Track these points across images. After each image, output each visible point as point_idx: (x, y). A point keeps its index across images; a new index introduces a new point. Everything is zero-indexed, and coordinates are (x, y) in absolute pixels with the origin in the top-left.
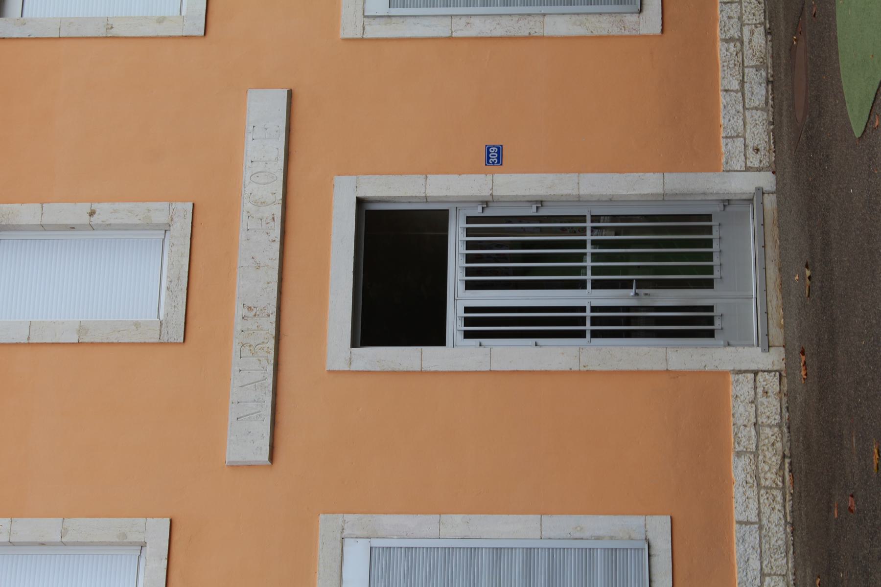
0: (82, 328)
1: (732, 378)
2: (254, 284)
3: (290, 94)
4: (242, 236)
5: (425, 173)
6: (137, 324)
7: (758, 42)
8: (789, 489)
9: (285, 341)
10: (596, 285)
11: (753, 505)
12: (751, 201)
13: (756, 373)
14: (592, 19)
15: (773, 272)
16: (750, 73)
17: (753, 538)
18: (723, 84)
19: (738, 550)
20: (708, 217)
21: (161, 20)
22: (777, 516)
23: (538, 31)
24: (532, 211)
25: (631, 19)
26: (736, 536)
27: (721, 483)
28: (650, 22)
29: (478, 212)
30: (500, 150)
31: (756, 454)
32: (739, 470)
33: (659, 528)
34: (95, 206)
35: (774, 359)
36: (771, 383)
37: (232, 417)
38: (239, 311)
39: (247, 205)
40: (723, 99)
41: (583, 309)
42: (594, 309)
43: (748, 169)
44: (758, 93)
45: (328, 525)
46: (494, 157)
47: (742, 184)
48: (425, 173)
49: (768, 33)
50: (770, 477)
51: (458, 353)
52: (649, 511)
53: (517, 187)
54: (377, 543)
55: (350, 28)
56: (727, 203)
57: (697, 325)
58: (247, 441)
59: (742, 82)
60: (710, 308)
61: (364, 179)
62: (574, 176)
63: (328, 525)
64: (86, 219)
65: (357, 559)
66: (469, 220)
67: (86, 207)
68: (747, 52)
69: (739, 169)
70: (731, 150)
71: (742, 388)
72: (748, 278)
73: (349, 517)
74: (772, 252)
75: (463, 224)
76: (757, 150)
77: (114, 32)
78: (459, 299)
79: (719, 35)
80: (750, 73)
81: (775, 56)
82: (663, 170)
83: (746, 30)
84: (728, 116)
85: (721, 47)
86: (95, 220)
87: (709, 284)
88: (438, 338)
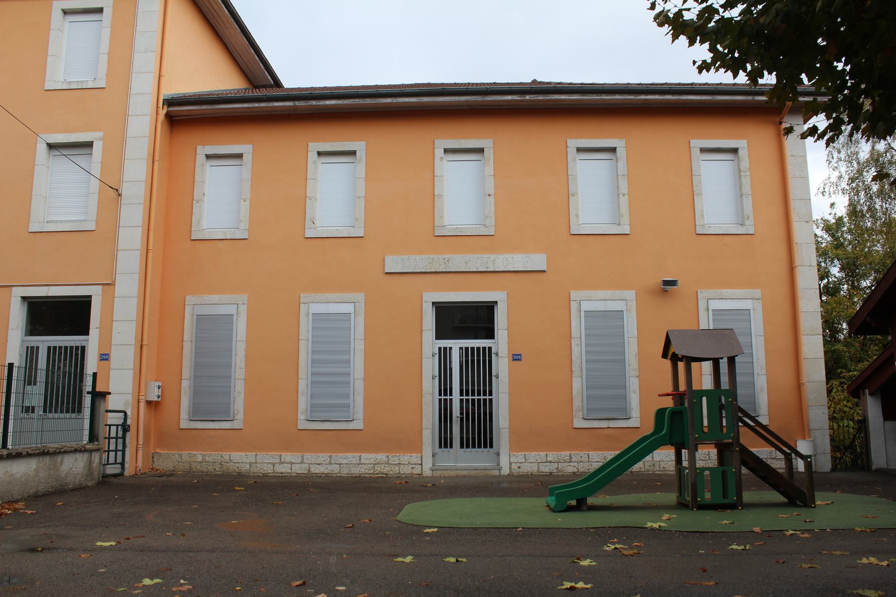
0: (440, 196)
1: (419, 455)
2: (458, 262)
3: (544, 271)
4: (479, 256)
5: (100, 328)
6: (442, 217)
7: (570, 469)
8: (374, 476)
9: (435, 276)
10: (461, 400)
11: (367, 462)
12: (499, 465)
13: (421, 464)
14: (580, 398)
15: (466, 473)
16: (556, 465)
17: (354, 461)
18: (550, 454)
19: (350, 455)
20: (491, 446)
21: (577, 216)
22: (363, 471)
23: (575, 375)
24: (494, 373)
25: (581, 415)
26: (542, 454)
27: (377, 449)
28: (579, 423)
29: (493, 351)
30: (520, 360)
31: (388, 463)
32: (381, 457)
33: (358, 425)
34: (493, 196)
35: (427, 472)
36: (417, 470)
37: (403, 257)
38: (447, 256)
39: (493, 257)
40: (543, 454)
41: (451, 395)
42: (451, 400)
43: (510, 464)
44: (545, 469)
45: (360, 297)
46: (516, 358)
47: (504, 461)
48: (508, 329)
49: (574, 473)
50: (378, 469)
51: (431, 344)
52: (365, 420)
53: (502, 366)
54: (235, 317)
55: (574, 295)
56: (498, 454)
57: (445, 442)
58: (393, 263)
59: (551, 462)
60: (451, 447)
61: (505, 304)
62: (507, 390)
63: (360, 297)
64: (621, 192)
65: (348, 308)
66: (490, 348)
67: (492, 192)
68: (565, 465)
69: (508, 459)
70: (519, 457)
71: (415, 458)
72: (465, 461)
73: (363, 304)
74: (473, 473)
75: (487, 346)
76: (519, 468)
77: (571, 198)
78: (456, 345)
79: (573, 453)
80: (556, 465)
81: (216, 475)
82: (510, 428)
83: (576, 464)
84: (533, 456)
85: (568, 453)
86: (621, 196)
87: (462, 446)
88: (439, 336)
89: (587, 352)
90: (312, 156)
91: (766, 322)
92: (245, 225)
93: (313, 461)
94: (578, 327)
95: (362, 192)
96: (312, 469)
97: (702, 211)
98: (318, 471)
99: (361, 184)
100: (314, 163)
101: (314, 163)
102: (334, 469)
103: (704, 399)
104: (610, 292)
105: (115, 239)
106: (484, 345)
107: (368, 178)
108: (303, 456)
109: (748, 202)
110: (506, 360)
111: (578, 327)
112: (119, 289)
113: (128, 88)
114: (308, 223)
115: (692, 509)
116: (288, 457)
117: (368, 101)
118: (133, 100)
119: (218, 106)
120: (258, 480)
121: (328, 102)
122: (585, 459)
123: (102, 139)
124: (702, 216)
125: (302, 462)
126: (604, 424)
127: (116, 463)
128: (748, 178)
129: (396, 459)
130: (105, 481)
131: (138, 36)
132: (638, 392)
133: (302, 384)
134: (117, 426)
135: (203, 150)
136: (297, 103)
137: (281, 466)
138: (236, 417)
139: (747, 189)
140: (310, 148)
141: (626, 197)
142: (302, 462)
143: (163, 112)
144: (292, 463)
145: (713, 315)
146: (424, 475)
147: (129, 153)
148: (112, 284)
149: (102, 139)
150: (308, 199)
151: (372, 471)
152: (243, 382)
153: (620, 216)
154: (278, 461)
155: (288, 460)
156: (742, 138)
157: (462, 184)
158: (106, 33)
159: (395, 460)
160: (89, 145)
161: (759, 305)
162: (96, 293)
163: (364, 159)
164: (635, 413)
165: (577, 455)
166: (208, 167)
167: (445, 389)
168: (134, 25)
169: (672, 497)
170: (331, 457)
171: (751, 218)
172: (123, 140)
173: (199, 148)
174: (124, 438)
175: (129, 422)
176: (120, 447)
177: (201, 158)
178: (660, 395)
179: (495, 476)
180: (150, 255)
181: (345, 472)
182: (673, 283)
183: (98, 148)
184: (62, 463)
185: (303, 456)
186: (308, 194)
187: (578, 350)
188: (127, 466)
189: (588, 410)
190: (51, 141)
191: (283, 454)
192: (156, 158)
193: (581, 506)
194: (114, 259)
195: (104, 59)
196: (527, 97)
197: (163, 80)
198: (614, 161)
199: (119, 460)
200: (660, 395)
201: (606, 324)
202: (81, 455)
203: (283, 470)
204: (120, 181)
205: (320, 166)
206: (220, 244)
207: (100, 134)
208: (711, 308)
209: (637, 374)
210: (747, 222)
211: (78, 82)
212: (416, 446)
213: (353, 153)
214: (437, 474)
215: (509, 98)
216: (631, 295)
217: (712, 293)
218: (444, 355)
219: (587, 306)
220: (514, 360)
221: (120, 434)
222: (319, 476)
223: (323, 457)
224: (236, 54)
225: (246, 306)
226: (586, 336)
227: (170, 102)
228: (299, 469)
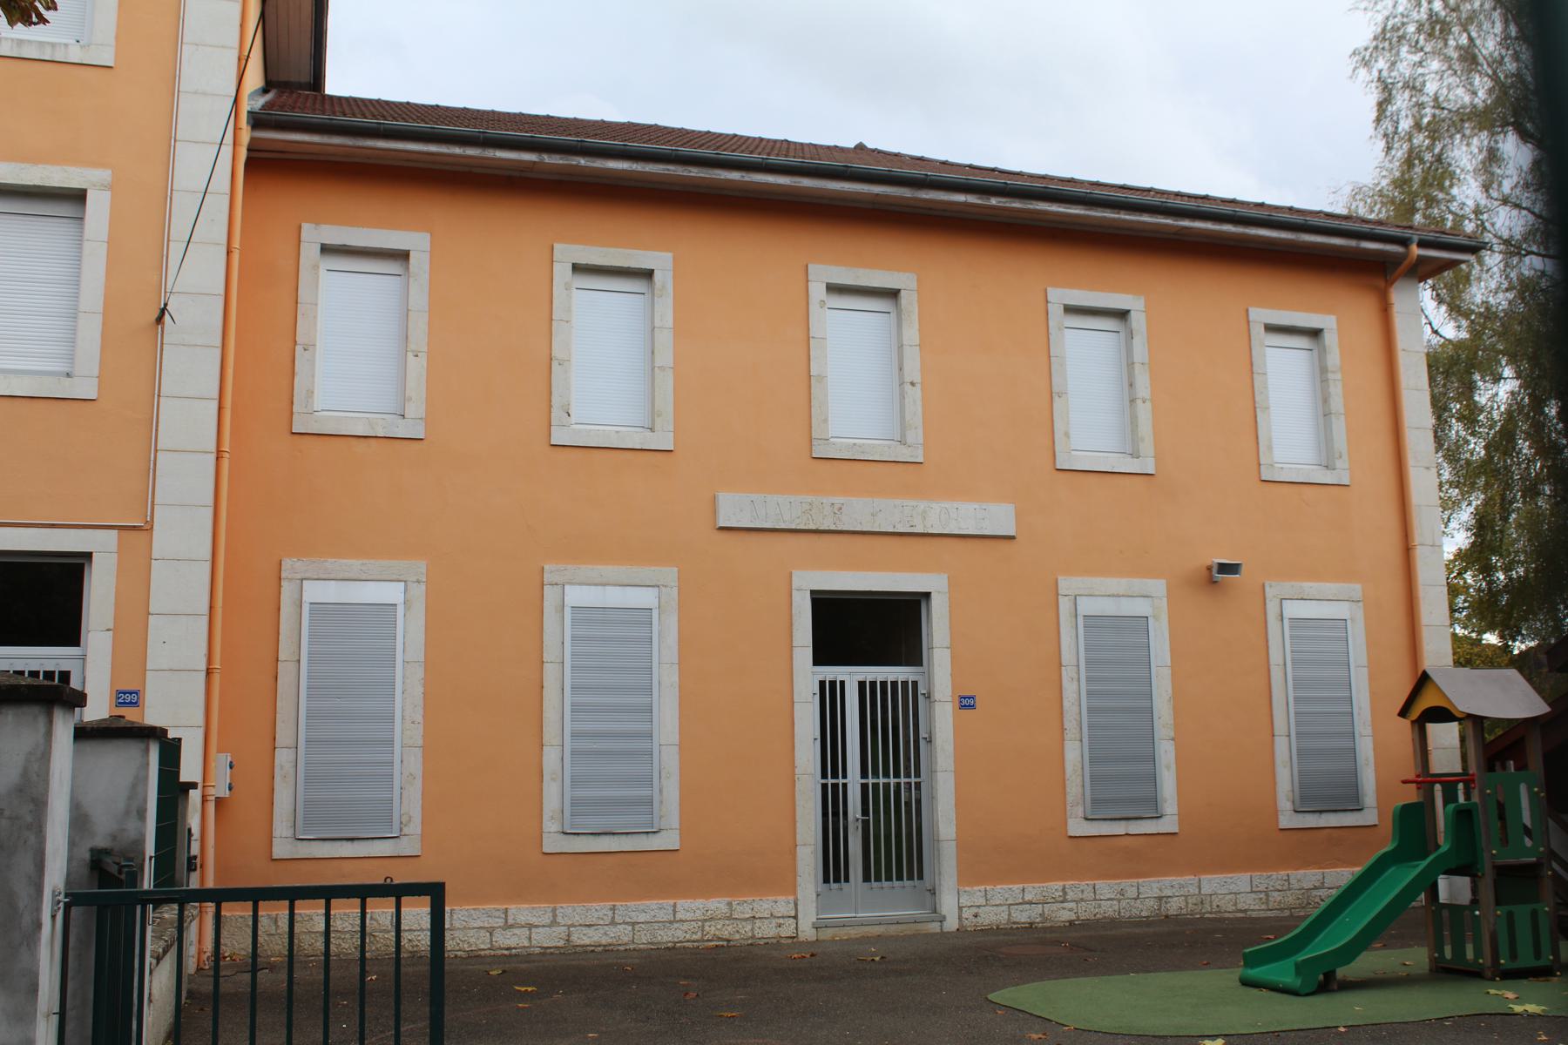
0: (822, 378)
1: (791, 898)
2: (861, 512)
3: (1012, 538)
4: (898, 502)
5: (115, 630)
6: (826, 421)
8: (702, 945)
10: (864, 787)
11: (689, 916)
13: (795, 917)
14: (1079, 780)
18: (1029, 887)
19: (653, 904)
20: (921, 877)
21: (1067, 435)
22: (680, 935)
23: (1069, 735)
24: (923, 734)
25: (1080, 811)
27: (706, 891)
28: (1078, 827)
29: (922, 690)
30: (972, 707)
31: (729, 918)
32: (717, 905)
33: (669, 840)
34: (918, 386)
35: (807, 932)
36: (788, 930)
37: (754, 496)
38: (838, 500)
39: (922, 505)
40: (1016, 887)
41: (845, 776)
42: (845, 785)
43: (960, 908)
44: (1022, 916)
45: (670, 574)
46: (966, 703)
47: (948, 904)
49: (1071, 922)
51: (807, 676)
52: (684, 832)
53: (942, 720)
54: (655, 614)
55: (1067, 584)
56: (933, 892)
57: (833, 869)
58: (735, 509)
59: (1031, 903)
60: (847, 880)
63: (670, 574)
64: (908, 379)
65: (390, 593)
66: (915, 684)
68: (1055, 907)
69: (961, 901)
70: (975, 895)
71: (783, 906)
72: (873, 911)
73: (675, 590)
76: (976, 916)
78: (851, 676)
83: (1072, 905)
85: (1058, 885)
86: (908, 387)
87: (866, 878)
88: (818, 660)
89: (1089, 693)
91: (1370, 644)
92: (416, 409)
93: (577, 919)
94: (1071, 647)
96: (574, 938)
97: (1270, 440)
98: (587, 942)
100: (568, 287)
101: (568, 287)
102: (620, 935)
103: (1438, 787)
104: (1124, 581)
105: (151, 423)
108: (554, 910)
109: (1339, 427)
110: (949, 708)
111: (1071, 647)
112: (162, 541)
114: (556, 414)
115: (1493, 979)
116: (521, 912)
117: (694, 172)
118: (186, 105)
121: (613, 164)
122: (1089, 895)
123: (111, 187)
124: (1270, 448)
125: (554, 923)
126: (1119, 828)
128: (1339, 385)
129: (747, 908)
132: (1174, 767)
133: (551, 758)
137: (509, 933)
138: (406, 831)
139: (1337, 403)
141: (1148, 404)
142: (554, 923)
144: (531, 926)
145: (1291, 628)
146: (802, 937)
148: (147, 529)
151: (697, 937)
152: (419, 752)
153: (405, 399)
154: (501, 922)
155: (522, 919)
156: (1329, 311)
157: (859, 351)
159: (743, 911)
161: (1360, 615)
162: (102, 547)
164: (1170, 806)
165: (1079, 888)
167: (831, 761)
169: (1417, 957)
170: (613, 909)
171: (1345, 456)
178: (1404, 782)
179: (933, 935)
180: (225, 464)
181: (643, 939)
182: (1226, 568)
183: (98, 206)
185: (554, 910)
187: (1073, 690)
189: (1094, 801)
191: (513, 908)
193: (1327, 983)
194: (149, 471)
196: (994, 201)
198: (893, 315)
200: (1404, 782)
201: (1117, 639)
203: (512, 942)
206: (360, 446)
207: (104, 175)
208: (1082, 610)
209: (1172, 734)
210: (1339, 464)
211: (41, 43)
212: (784, 882)
214: (827, 934)
215: (960, 198)
216: (1158, 587)
217: (1287, 587)
218: (830, 695)
219: (1088, 607)
220: (963, 707)
222: (587, 951)
223: (598, 910)
225: (423, 587)
226: (1088, 662)
228: (547, 938)
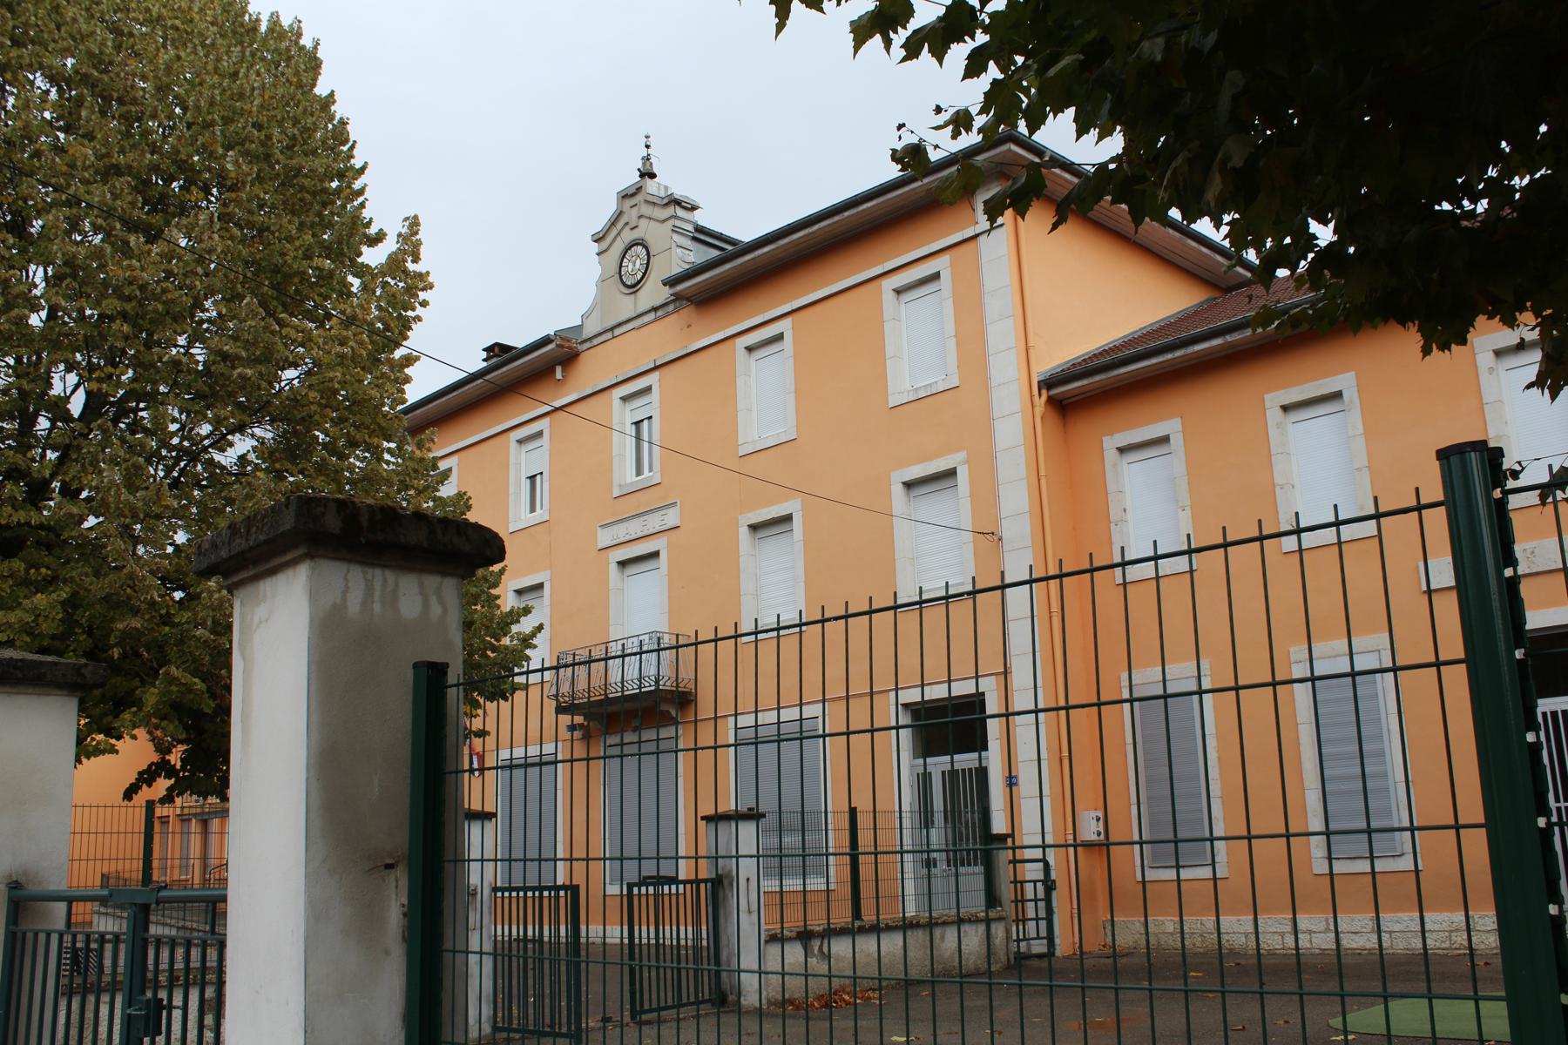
11: (1436, 927)
90: (1274, 415)
95: (1363, 460)
99: (1360, 444)
101: (1279, 426)
106: (1553, 708)
107: (1369, 432)
113: (986, 379)
119: (1116, 372)
120: (1243, 962)
123: (967, 461)
127: (1038, 938)
130: (1020, 962)
131: (987, 298)
134: (1035, 882)
135: (1111, 443)
136: (1229, 338)
140: (1268, 404)
143: (1041, 402)
147: (1003, 475)
149: (967, 461)
150: (1278, 490)
151: (1447, 945)
158: (948, 305)
160: (951, 473)
163: (1357, 401)
166: (1125, 466)
168: (979, 285)
172: (991, 457)
173: (1106, 439)
174: (1048, 900)
175: (1053, 876)
176: (1042, 914)
177: (1111, 455)
183: (963, 474)
184: (943, 938)
186: (1278, 480)
188: (1057, 941)
190: (907, 479)
192: (1042, 473)
195: (952, 344)
197: (1031, 352)
199: (1043, 933)
202: (974, 927)
204: (997, 520)
205: (1291, 428)
207: (962, 455)
213: (1337, 396)
221: (1041, 894)
224: (1169, 256)
227: (1048, 383)
